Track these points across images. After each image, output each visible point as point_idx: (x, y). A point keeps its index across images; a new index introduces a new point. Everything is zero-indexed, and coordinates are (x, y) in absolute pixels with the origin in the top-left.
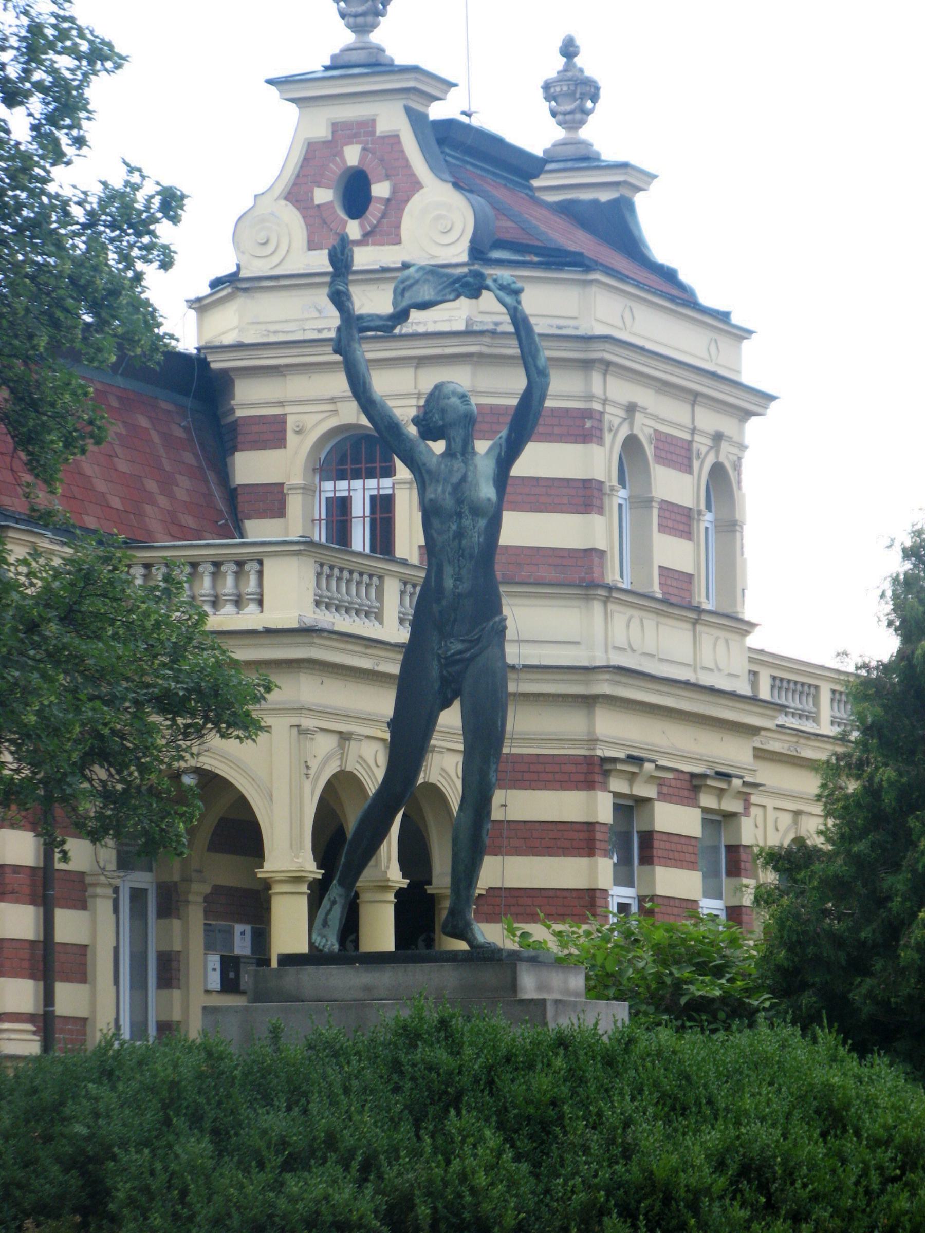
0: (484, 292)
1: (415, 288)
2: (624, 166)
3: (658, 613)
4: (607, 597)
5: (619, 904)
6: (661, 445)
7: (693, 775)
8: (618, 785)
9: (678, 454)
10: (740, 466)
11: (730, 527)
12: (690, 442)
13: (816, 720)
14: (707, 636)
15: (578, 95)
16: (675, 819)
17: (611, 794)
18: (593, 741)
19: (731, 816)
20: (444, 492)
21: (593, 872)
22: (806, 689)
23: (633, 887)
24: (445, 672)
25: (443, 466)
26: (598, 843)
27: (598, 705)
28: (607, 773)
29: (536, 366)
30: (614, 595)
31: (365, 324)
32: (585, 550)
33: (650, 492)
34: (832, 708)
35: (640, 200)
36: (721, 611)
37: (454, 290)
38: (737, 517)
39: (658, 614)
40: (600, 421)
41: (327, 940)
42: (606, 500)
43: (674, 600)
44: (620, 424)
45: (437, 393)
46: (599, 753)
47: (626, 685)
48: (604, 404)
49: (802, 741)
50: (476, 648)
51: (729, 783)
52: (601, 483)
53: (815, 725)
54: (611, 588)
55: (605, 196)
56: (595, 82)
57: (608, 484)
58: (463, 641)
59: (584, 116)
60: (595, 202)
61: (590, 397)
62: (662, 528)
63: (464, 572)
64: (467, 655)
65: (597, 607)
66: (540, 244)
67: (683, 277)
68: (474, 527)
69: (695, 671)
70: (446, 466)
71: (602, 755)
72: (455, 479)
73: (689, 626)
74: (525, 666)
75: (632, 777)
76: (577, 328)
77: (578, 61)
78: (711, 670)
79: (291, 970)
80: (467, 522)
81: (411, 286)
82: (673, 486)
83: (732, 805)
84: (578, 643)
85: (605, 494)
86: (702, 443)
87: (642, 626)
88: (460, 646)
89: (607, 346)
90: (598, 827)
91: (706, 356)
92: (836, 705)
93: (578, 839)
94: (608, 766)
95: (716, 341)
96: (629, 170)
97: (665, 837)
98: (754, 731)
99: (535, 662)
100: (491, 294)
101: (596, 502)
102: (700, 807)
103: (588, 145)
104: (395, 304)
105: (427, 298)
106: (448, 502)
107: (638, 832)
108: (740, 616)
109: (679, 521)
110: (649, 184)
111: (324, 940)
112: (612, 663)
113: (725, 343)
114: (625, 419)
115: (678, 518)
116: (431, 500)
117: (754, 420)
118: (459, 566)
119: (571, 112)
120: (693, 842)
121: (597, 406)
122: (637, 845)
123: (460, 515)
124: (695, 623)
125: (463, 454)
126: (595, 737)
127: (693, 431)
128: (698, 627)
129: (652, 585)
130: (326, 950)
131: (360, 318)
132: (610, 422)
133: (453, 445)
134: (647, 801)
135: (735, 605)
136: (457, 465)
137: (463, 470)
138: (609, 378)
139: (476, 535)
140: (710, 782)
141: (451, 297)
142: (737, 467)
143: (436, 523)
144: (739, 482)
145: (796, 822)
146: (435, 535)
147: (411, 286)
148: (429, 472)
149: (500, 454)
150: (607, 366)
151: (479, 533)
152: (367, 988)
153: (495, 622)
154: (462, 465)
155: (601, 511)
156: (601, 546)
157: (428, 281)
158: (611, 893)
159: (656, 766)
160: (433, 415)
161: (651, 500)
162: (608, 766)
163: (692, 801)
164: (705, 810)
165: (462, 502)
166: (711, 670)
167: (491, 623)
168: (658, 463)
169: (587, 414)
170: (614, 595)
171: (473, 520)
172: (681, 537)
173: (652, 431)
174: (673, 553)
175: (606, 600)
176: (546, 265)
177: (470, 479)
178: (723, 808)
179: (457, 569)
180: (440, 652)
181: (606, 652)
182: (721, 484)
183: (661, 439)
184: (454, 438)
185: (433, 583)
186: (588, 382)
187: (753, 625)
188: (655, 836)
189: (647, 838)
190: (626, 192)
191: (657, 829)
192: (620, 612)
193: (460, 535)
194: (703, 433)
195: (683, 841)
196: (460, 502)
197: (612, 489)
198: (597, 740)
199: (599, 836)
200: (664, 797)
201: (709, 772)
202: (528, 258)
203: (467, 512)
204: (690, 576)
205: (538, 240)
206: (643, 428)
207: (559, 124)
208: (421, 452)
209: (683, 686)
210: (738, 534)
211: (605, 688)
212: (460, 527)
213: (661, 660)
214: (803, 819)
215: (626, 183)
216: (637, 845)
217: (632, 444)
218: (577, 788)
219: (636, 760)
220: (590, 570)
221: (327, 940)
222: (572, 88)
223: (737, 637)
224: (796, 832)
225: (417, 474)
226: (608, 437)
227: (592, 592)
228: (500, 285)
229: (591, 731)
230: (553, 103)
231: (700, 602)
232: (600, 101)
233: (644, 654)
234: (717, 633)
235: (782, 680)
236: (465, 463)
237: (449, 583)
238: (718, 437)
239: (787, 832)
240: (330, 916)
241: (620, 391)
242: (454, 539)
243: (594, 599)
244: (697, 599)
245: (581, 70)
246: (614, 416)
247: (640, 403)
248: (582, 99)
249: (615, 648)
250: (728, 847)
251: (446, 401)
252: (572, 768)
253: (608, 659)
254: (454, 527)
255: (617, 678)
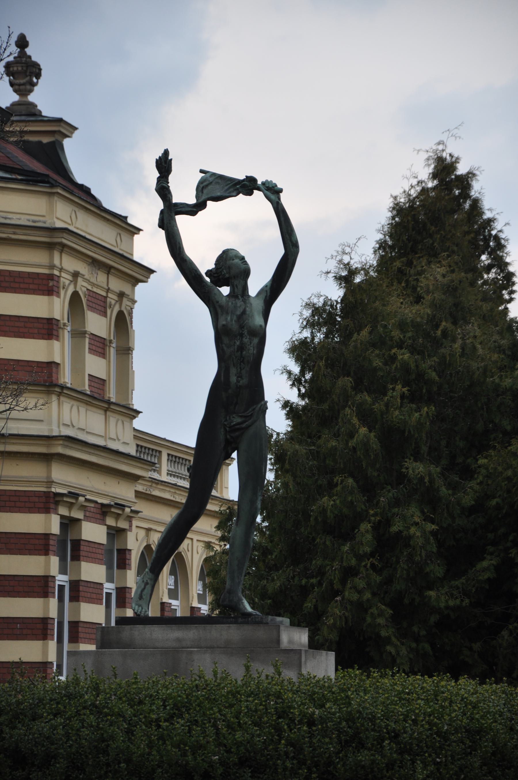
0: (255, 191)
1: (210, 187)
2: (60, 121)
3: (87, 403)
4: (60, 392)
5: (59, 585)
6: (90, 299)
7: (102, 505)
8: (63, 511)
9: (100, 305)
10: (132, 313)
11: (126, 351)
12: (106, 297)
13: (159, 472)
14: (113, 419)
15: (28, 74)
16: (93, 532)
17: (59, 516)
18: (50, 482)
19: (123, 531)
20: (231, 320)
21: (48, 565)
22: (154, 453)
23: (67, 575)
24: (228, 436)
25: (230, 304)
26: (51, 546)
27: (53, 460)
28: (57, 503)
29: (291, 240)
30: (65, 391)
31: (179, 210)
32: (48, 363)
33: (84, 327)
34: (167, 466)
35: (67, 143)
36: (118, 402)
37: (235, 190)
38: (130, 345)
39: (87, 404)
40: (58, 282)
41: (142, 609)
42: (61, 331)
43: (96, 395)
44: (69, 284)
45: (225, 256)
46: (53, 490)
47: (71, 448)
48: (60, 272)
49: (154, 485)
50: (250, 421)
51: (123, 510)
52: (58, 321)
53: (158, 475)
54: (63, 387)
55: (45, 140)
56: (39, 65)
57: (62, 322)
58: (241, 416)
59: (32, 87)
60: (40, 142)
61: (52, 267)
62: (92, 351)
63: (244, 372)
64: (244, 425)
65: (54, 398)
66: (20, 167)
67: (93, 192)
68: (251, 343)
69: (106, 441)
70: (232, 303)
71: (54, 491)
72: (238, 313)
73: (102, 412)
74: (11, 435)
75: (71, 506)
76: (45, 223)
77: (29, 51)
78: (114, 440)
79: (127, 627)
80: (246, 340)
81: (207, 186)
82: (97, 324)
83: (122, 524)
84: (42, 421)
85: (60, 328)
86: (112, 298)
87: (79, 411)
88: (239, 420)
89: (65, 235)
90: (51, 537)
91: (115, 244)
92: (169, 463)
93: (37, 544)
94: (58, 499)
95: (120, 234)
96: (62, 124)
97: (86, 544)
98: (135, 478)
99: (15, 432)
100: (261, 193)
101: (55, 333)
102: (106, 525)
103: (34, 105)
104: (197, 197)
105: (219, 194)
106: (235, 327)
107: (70, 540)
108: (131, 406)
109: (100, 347)
110: (72, 133)
111: (140, 608)
112: (62, 434)
113: (125, 236)
114: (71, 281)
115: (98, 344)
116: (224, 325)
117: (140, 285)
118: (240, 368)
119: (24, 84)
120: (102, 547)
121: (56, 273)
122: (72, 548)
123: (242, 335)
124: (106, 410)
125: (242, 297)
126: (50, 480)
127: (108, 290)
128: (108, 413)
129: (84, 386)
130: (142, 615)
131: (176, 204)
132: (64, 283)
133: (236, 290)
134: (78, 520)
135: (128, 400)
136: (239, 303)
137: (243, 307)
138: (64, 255)
139: (252, 348)
140: (113, 510)
141: (234, 194)
142: (131, 314)
143: (226, 340)
144: (131, 323)
145: (147, 535)
146: (225, 348)
147: (207, 186)
148: (221, 307)
149: (266, 296)
150: (63, 248)
151: (254, 348)
152: (178, 640)
153: (262, 405)
154: (242, 303)
155: (57, 338)
156: (57, 360)
157: (218, 183)
158: (57, 578)
159: (86, 498)
160: (222, 270)
161: (85, 332)
162: (58, 499)
163: (102, 522)
164: (109, 527)
165: (243, 327)
166: (114, 440)
167: (259, 406)
168: (88, 310)
169: (51, 277)
170: (65, 391)
171: (250, 339)
172: (100, 356)
173: (85, 289)
174: (95, 366)
175: (59, 395)
176: (26, 182)
177: (248, 313)
178: (119, 525)
179: (239, 370)
180: (226, 423)
181: (59, 427)
182: (123, 323)
183: (90, 294)
184: (237, 286)
185: (222, 378)
186: (52, 257)
187: (138, 412)
188: (82, 543)
189: (77, 544)
190: (58, 137)
191: (83, 538)
192: (66, 402)
193: (241, 348)
194: (113, 292)
195: (96, 546)
196: (242, 327)
197: (64, 325)
198: (53, 482)
199: (51, 542)
200: (87, 518)
201: (112, 503)
202: (14, 177)
203: (246, 333)
204: (104, 381)
205: (19, 165)
206: (82, 286)
207: (15, 91)
208: (215, 294)
209: (102, 449)
210: (130, 355)
211: (60, 450)
212: (242, 343)
213: (87, 432)
214: (152, 533)
215: (60, 132)
216: (72, 548)
217: (75, 297)
218: (39, 512)
219: (75, 496)
220: (50, 375)
221: (142, 609)
222: (25, 68)
223: (128, 420)
224: (147, 542)
225: (212, 309)
226: (62, 292)
227: (51, 389)
228: (267, 187)
229: (49, 476)
230: (11, 78)
231: (109, 397)
232: (41, 78)
233: (79, 429)
234: (117, 416)
235: (142, 447)
236: (244, 301)
237: (233, 379)
238: (121, 295)
239: (142, 541)
240: (143, 593)
241: (70, 264)
242: (238, 351)
243: (52, 393)
244: (108, 395)
245: (30, 57)
246: (65, 278)
247: (81, 272)
248: (30, 76)
249: (64, 425)
250: (119, 551)
251: (231, 261)
252: (36, 499)
253: (60, 431)
254: (238, 343)
255: (66, 443)
